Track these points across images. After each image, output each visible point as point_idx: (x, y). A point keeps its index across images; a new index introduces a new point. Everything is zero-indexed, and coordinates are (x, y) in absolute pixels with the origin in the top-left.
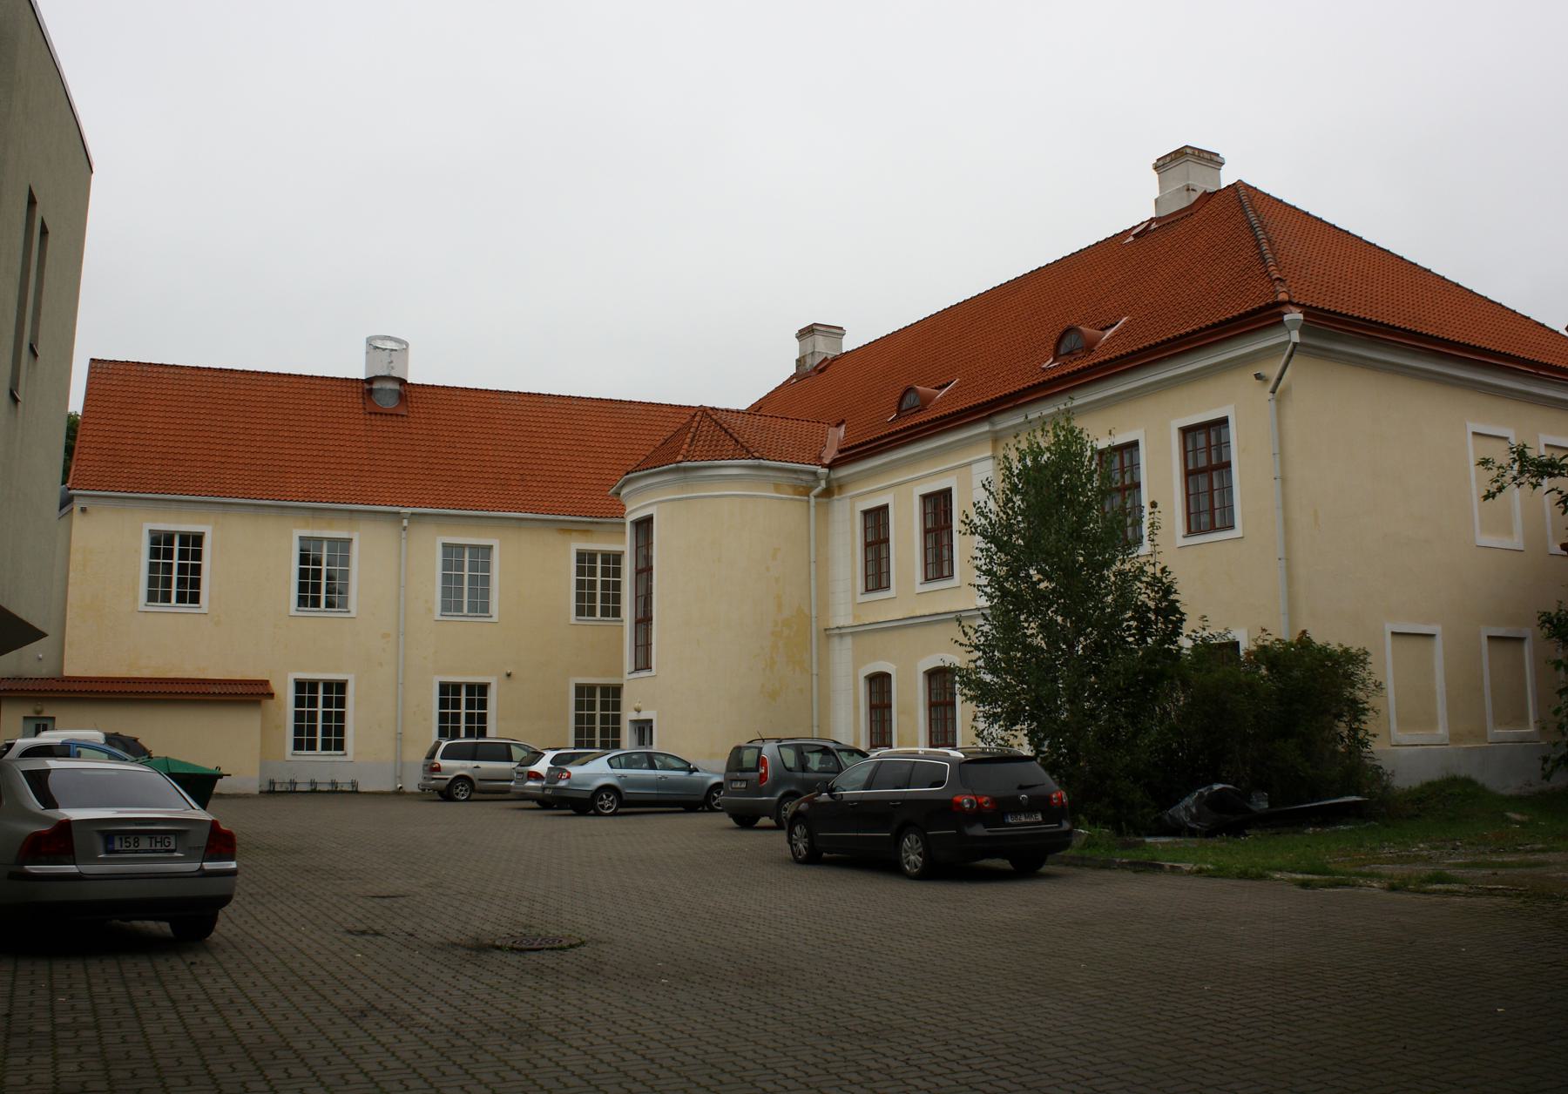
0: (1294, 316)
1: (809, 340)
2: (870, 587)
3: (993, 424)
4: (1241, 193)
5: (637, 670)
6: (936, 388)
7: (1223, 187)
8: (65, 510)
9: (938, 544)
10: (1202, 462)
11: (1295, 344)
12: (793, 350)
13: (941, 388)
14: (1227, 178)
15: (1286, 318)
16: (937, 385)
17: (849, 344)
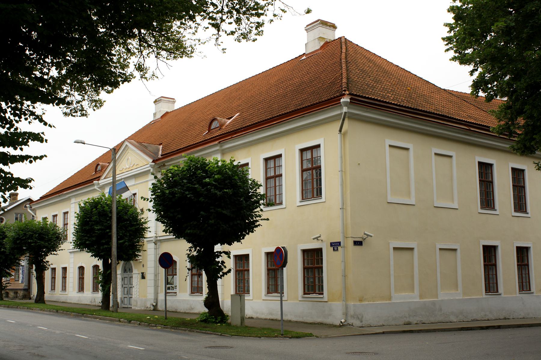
0: (345, 99)
1: (160, 105)
2: (525, 250)
3: (221, 146)
4: (343, 42)
5: (52, 290)
6: (227, 119)
7: (336, 38)
8: (203, 324)
9: (519, 192)
10: (272, 174)
11: (345, 113)
12: (152, 108)
13: (229, 119)
14: (338, 34)
15: (342, 100)
16: (227, 118)
17: (177, 106)
